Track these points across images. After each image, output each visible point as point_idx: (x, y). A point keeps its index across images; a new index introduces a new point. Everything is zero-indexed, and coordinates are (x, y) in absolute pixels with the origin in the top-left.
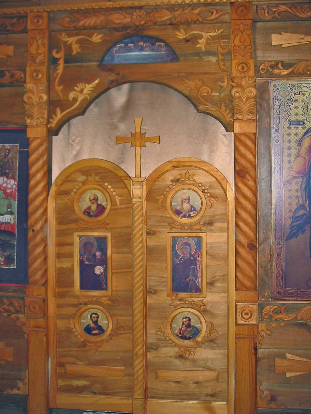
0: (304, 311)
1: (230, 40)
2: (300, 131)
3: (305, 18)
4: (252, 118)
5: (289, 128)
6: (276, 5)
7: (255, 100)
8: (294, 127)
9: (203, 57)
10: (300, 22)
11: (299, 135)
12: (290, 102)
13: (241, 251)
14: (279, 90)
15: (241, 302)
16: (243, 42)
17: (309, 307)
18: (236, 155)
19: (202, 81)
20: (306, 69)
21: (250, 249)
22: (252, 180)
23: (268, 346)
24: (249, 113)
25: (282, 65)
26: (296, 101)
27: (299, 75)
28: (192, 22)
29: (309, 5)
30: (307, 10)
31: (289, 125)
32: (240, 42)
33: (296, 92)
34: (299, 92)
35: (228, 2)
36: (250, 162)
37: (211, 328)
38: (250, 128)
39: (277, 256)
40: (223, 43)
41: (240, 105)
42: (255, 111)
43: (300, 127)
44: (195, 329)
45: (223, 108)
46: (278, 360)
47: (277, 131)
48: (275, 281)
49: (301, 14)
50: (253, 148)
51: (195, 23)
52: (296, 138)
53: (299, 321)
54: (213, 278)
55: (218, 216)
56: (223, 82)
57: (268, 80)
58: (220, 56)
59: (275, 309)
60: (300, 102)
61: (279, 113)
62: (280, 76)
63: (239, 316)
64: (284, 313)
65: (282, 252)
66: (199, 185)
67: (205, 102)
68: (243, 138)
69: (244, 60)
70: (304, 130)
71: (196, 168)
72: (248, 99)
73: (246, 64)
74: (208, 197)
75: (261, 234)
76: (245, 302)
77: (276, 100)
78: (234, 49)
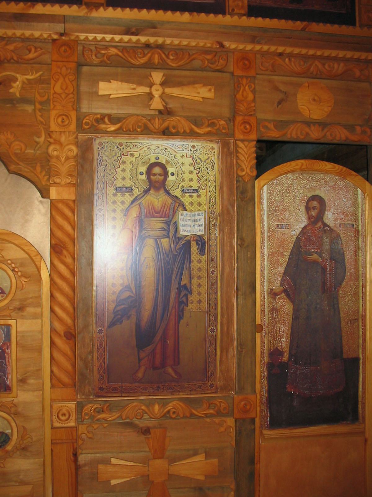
0: (129, 408)
1: (50, 86)
2: (127, 199)
3: (138, 65)
4: (71, 182)
5: (115, 195)
6: (106, 47)
7: (76, 159)
8: (120, 193)
9: (18, 105)
10: (132, 69)
11: (125, 203)
12: (116, 164)
13: (58, 341)
14: (104, 149)
15: (57, 401)
16: (65, 89)
17: (135, 404)
18: (52, 226)
19: (15, 134)
20: (137, 126)
21: (68, 339)
22: (69, 256)
23: (90, 451)
24: (67, 176)
25: (110, 120)
26: (124, 162)
27: (128, 132)
28: (6, 61)
29: (143, 50)
30: (140, 56)
31: (114, 191)
32: (62, 88)
33: (124, 152)
34: (128, 152)
35: (49, 38)
36: (68, 235)
37: (24, 433)
38: (69, 194)
39: (98, 346)
40: (41, 89)
41: (58, 166)
42: (75, 174)
43: (127, 194)
44: (4, 436)
45: (38, 169)
46: (101, 467)
47: (100, 199)
48: (97, 375)
49: (134, 60)
50: (72, 219)
51: (9, 61)
52: (123, 207)
53: (124, 420)
54: (25, 374)
55: (31, 300)
56: (39, 137)
57: (92, 137)
58: (37, 104)
59: (97, 408)
60: (128, 165)
61: (104, 176)
62: (106, 132)
63: (55, 418)
64: (107, 412)
65: (104, 341)
66: (8, 261)
67: (17, 161)
68: (60, 205)
69: (65, 111)
70: (132, 197)
71: (4, 242)
72: (67, 158)
73: (66, 116)
74: (19, 276)
75: (80, 320)
76: (63, 400)
77: (100, 161)
78: (54, 98)
